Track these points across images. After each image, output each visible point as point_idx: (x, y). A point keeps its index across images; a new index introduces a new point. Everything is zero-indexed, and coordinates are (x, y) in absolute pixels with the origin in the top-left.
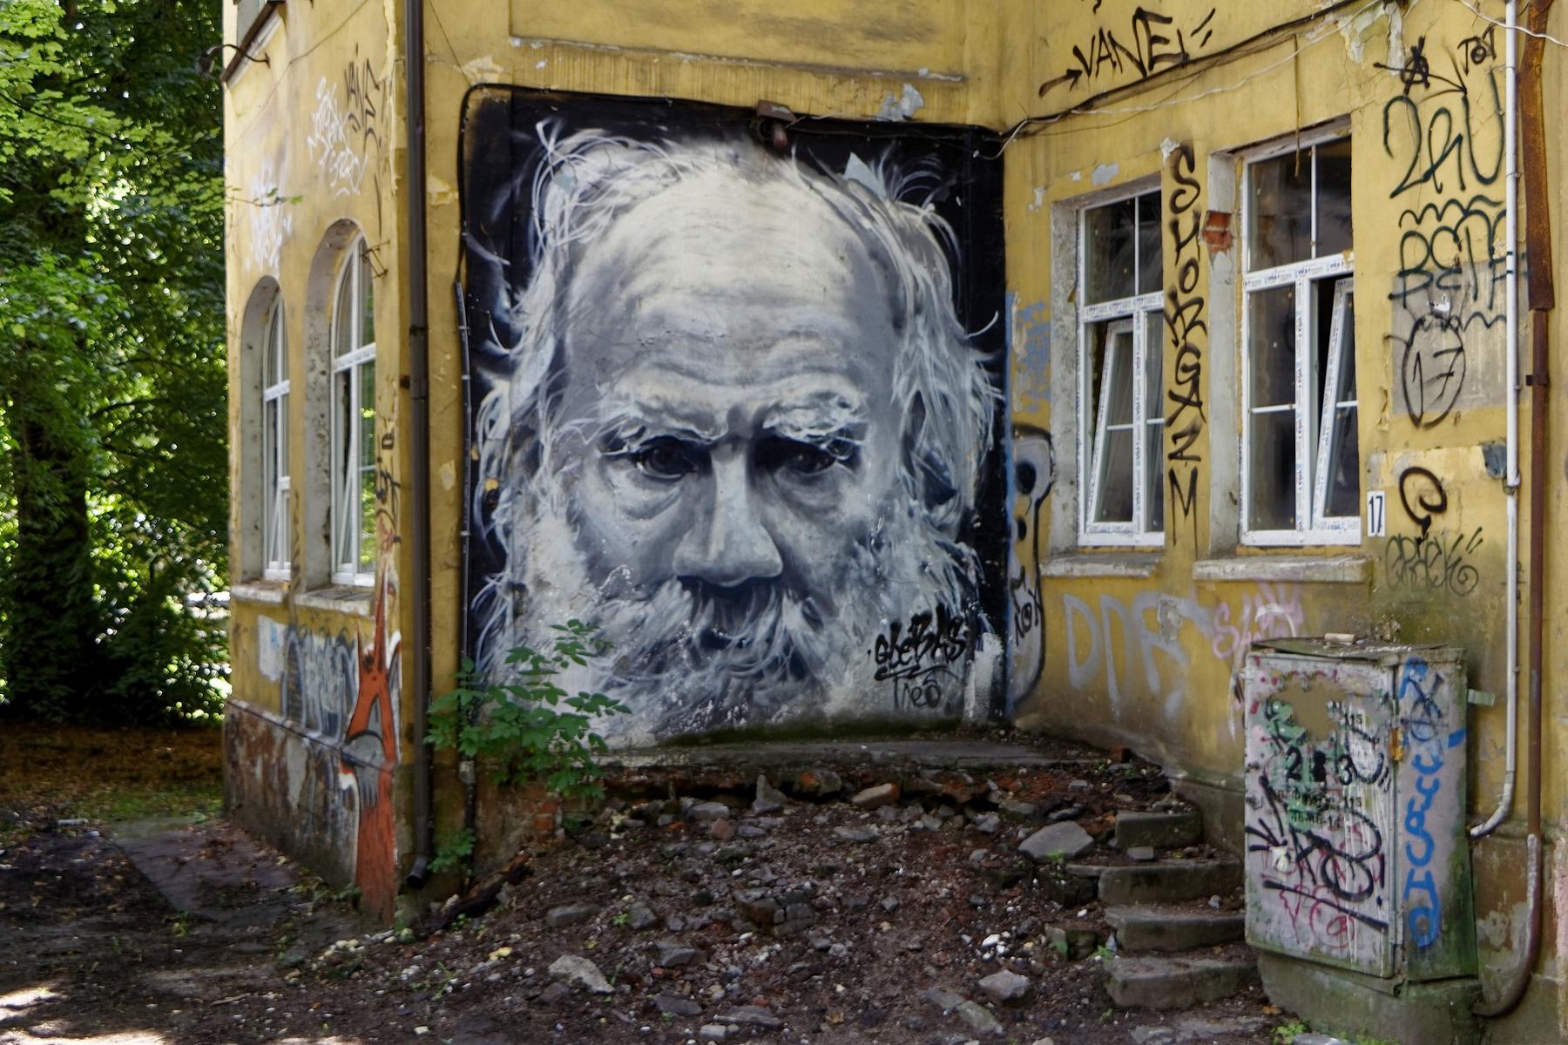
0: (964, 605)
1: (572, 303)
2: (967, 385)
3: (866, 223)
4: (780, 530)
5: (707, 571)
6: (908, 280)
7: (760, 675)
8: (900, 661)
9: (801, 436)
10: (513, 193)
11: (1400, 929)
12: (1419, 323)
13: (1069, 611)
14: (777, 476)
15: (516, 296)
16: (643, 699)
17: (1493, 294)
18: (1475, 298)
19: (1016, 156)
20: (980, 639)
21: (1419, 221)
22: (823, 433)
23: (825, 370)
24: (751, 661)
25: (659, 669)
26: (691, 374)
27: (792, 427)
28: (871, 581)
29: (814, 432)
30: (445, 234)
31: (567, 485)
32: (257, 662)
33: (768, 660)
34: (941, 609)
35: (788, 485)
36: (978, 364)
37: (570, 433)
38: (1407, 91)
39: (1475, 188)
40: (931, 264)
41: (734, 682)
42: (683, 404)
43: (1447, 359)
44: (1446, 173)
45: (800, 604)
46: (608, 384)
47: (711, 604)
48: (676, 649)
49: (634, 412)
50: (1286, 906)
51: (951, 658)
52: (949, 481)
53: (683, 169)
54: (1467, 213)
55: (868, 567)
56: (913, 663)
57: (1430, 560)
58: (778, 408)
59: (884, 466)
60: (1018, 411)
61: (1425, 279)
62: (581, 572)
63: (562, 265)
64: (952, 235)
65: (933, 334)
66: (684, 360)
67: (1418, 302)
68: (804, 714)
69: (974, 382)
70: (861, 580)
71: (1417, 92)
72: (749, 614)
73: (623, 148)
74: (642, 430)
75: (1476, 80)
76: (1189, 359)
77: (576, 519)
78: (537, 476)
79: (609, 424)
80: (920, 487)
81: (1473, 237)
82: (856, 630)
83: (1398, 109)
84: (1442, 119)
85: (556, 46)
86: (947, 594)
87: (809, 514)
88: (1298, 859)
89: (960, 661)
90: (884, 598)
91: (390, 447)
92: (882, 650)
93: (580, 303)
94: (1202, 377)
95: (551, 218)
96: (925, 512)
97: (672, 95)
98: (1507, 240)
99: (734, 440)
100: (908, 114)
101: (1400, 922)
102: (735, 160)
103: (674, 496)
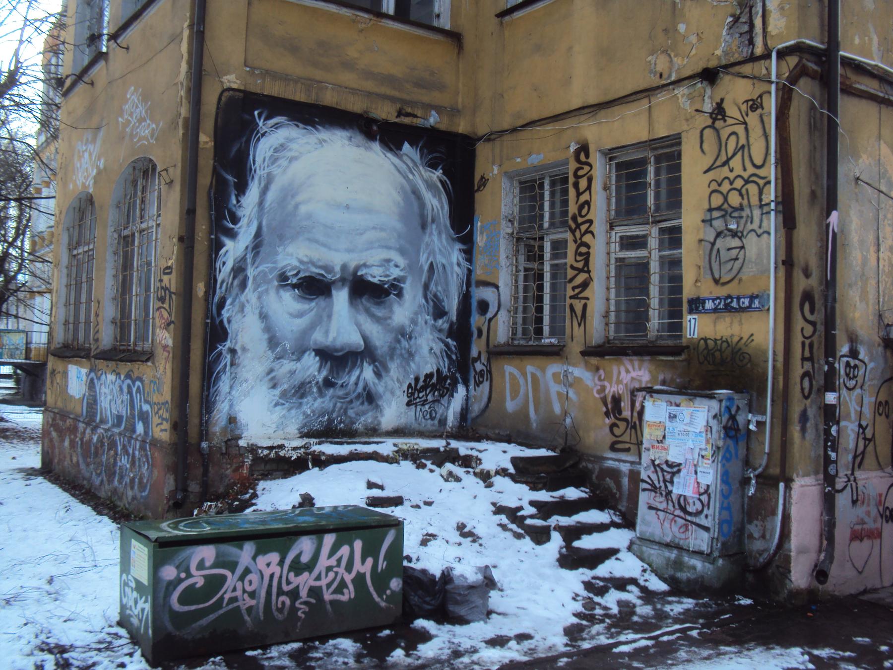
0: (449, 369)
1: (267, 204)
2: (455, 261)
3: (411, 176)
4: (364, 327)
5: (327, 347)
6: (429, 206)
7: (351, 402)
8: (418, 397)
9: (375, 280)
10: (241, 145)
11: (717, 530)
12: (719, 234)
13: (507, 374)
14: (363, 300)
15: (239, 198)
16: (293, 412)
17: (761, 221)
18: (752, 222)
19: (483, 151)
20: (456, 387)
21: (720, 185)
22: (386, 279)
23: (389, 248)
24: (347, 394)
25: (302, 396)
26: (324, 245)
27: (371, 275)
28: (406, 356)
29: (382, 279)
30: (207, 162)
31: (259, 298)
32: (67, 389)
33: (355, 394)
34: (438, 370)
35: (368, 305)
36: (460, 250)
37: (262, 271)
38: (713, 123)
39: (751, 170)
40: (440, 200)
41: (339, 405)
42: (319, 260)
43: (734, 252)
44: (736, 163)
45: (372, 366)
46: (282, 247)
47: (329, 364)
48: (311, 386)
49: (295, 263)
50: (659, 518)
51: (442, 396)
52: (444, 308)
53: (325, 141)
54: (747, 182)
55: (405, 348)
56: (424, 398)
57: (723, 349)
58: (365, 265)
59: (415, 297)
60: (479, 273)
61: (723, 213)
62: (264, 345)
63: (263, 184)
64: (450, 186)
65: (440, 234)
66: (322, 239)
67: (719, 224)
68: (372, 422)
69: (458, 259)
70: (401, 355)
71: (719, 124)
72: (347, 370)
73: (296, 128)
74: (298, 272)
75: (753, 119)
76: (583, 250)
77: (263, 317)
78: (245, 293)
79: (282, 268)
80: (431, 309)
81: (750, 193)
82: (398, 380)
83: (707, 132)
84: (733, 138)
85: (267, 73)
86: (441, 364)
87: (377, 320)
88: (666, 496)
89: (446, 397)
90: (412, 364)
91: (170, 273)
92: (410, 391)
93: (270, 204)
94: (591, 258)
95: (259, 160)
96: (433, 322)
97: (321, 104)
98: (771, 194)
99: (343, 280)
100: (432, 124)
101: (717, 526)
102: (350, 139)
103: (313, 306)
